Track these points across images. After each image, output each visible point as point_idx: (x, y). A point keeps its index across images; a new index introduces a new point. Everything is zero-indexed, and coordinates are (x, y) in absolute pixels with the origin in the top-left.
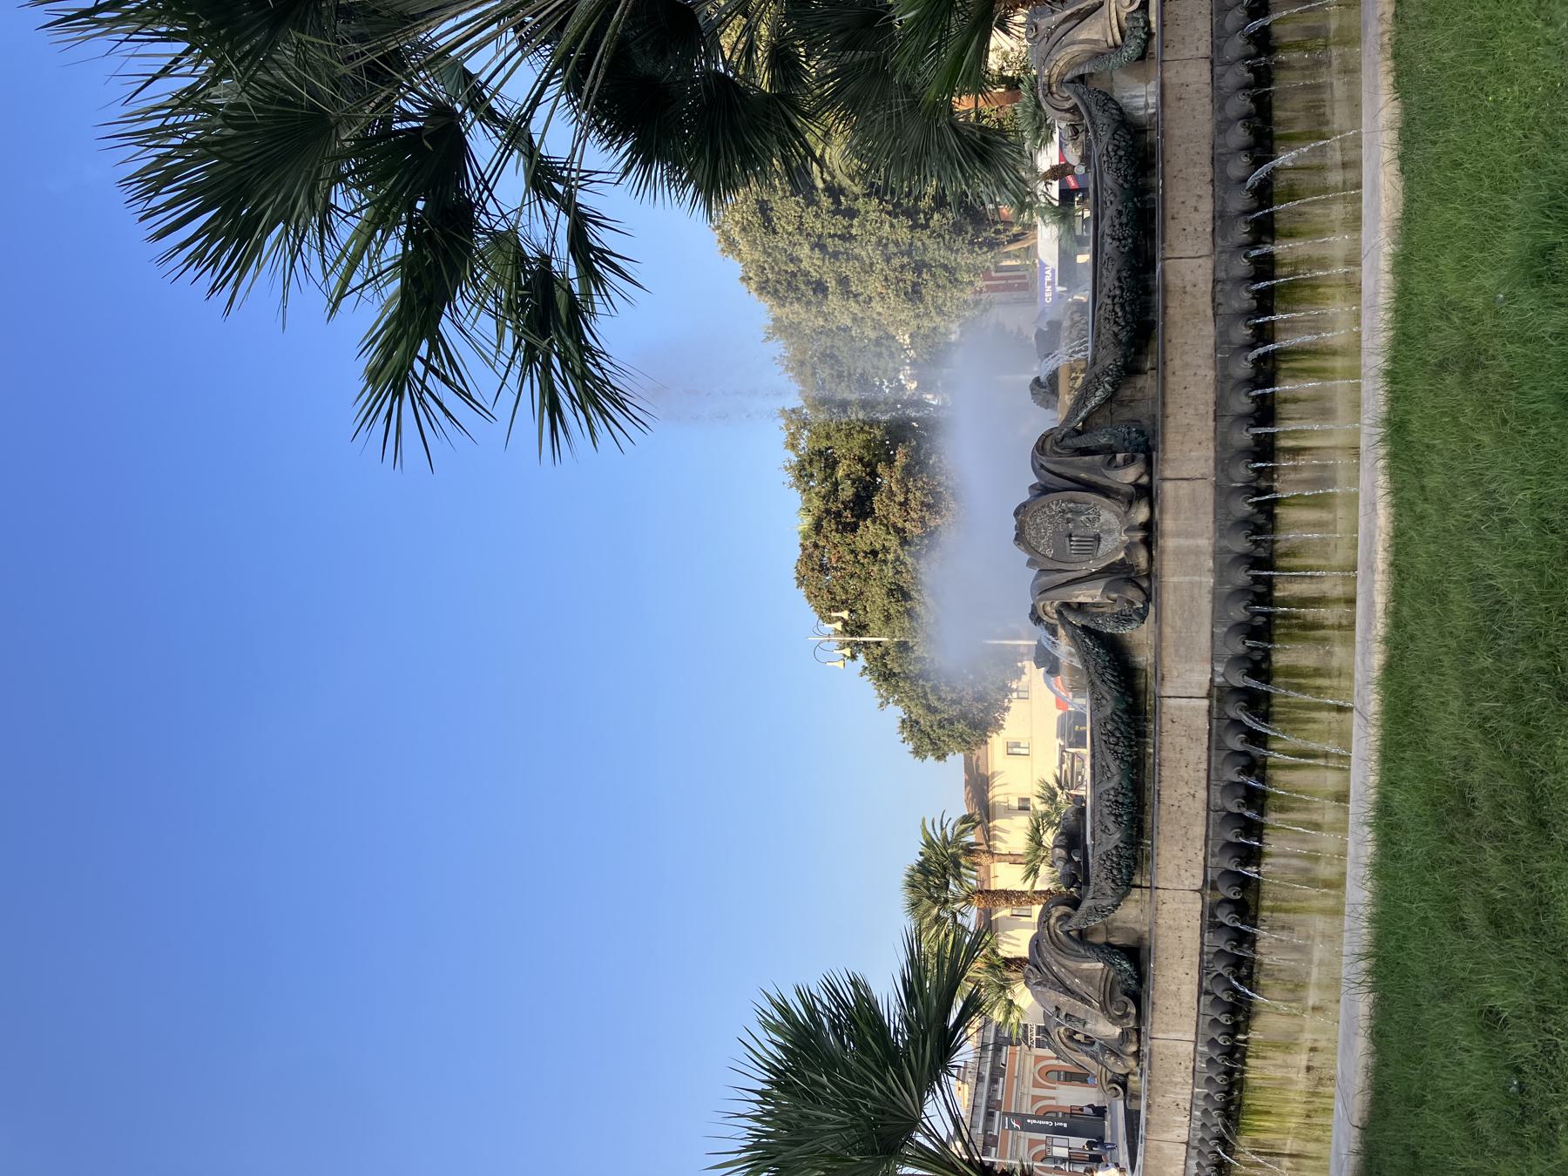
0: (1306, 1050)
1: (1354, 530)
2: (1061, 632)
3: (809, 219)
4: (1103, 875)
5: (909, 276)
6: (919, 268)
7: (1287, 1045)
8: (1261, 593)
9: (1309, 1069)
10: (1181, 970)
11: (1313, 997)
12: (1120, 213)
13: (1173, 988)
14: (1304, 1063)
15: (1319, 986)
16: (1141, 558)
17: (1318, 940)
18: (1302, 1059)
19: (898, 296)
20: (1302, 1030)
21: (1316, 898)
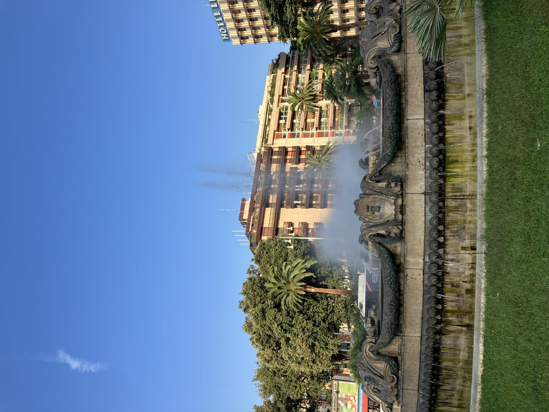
0: (468, 118)
1: (473, 174)
2: (370, 243)
3: (278, 316)
4: (385, 331)
5: (311, 340)
6: (315, 339)
7: (460, 117)
8: (442, 153)
9: (470, 128)
10: (417, 84)
11: (467, 90)
12: (392, 102)
13: (414, 93)
14: (468, 125)
15: (469, 84)
16: (400, 217)
17: (465, 65)
18: (466, 123)
19: (306, 346)
20: (465, 107)
21: (463, 50)
